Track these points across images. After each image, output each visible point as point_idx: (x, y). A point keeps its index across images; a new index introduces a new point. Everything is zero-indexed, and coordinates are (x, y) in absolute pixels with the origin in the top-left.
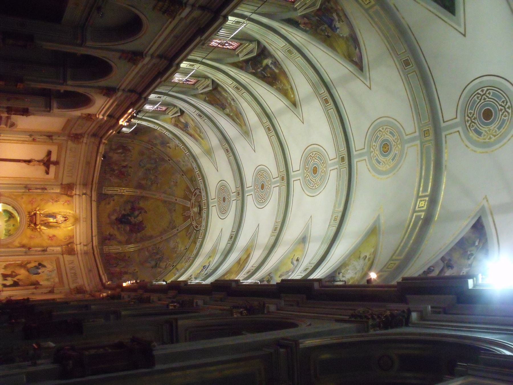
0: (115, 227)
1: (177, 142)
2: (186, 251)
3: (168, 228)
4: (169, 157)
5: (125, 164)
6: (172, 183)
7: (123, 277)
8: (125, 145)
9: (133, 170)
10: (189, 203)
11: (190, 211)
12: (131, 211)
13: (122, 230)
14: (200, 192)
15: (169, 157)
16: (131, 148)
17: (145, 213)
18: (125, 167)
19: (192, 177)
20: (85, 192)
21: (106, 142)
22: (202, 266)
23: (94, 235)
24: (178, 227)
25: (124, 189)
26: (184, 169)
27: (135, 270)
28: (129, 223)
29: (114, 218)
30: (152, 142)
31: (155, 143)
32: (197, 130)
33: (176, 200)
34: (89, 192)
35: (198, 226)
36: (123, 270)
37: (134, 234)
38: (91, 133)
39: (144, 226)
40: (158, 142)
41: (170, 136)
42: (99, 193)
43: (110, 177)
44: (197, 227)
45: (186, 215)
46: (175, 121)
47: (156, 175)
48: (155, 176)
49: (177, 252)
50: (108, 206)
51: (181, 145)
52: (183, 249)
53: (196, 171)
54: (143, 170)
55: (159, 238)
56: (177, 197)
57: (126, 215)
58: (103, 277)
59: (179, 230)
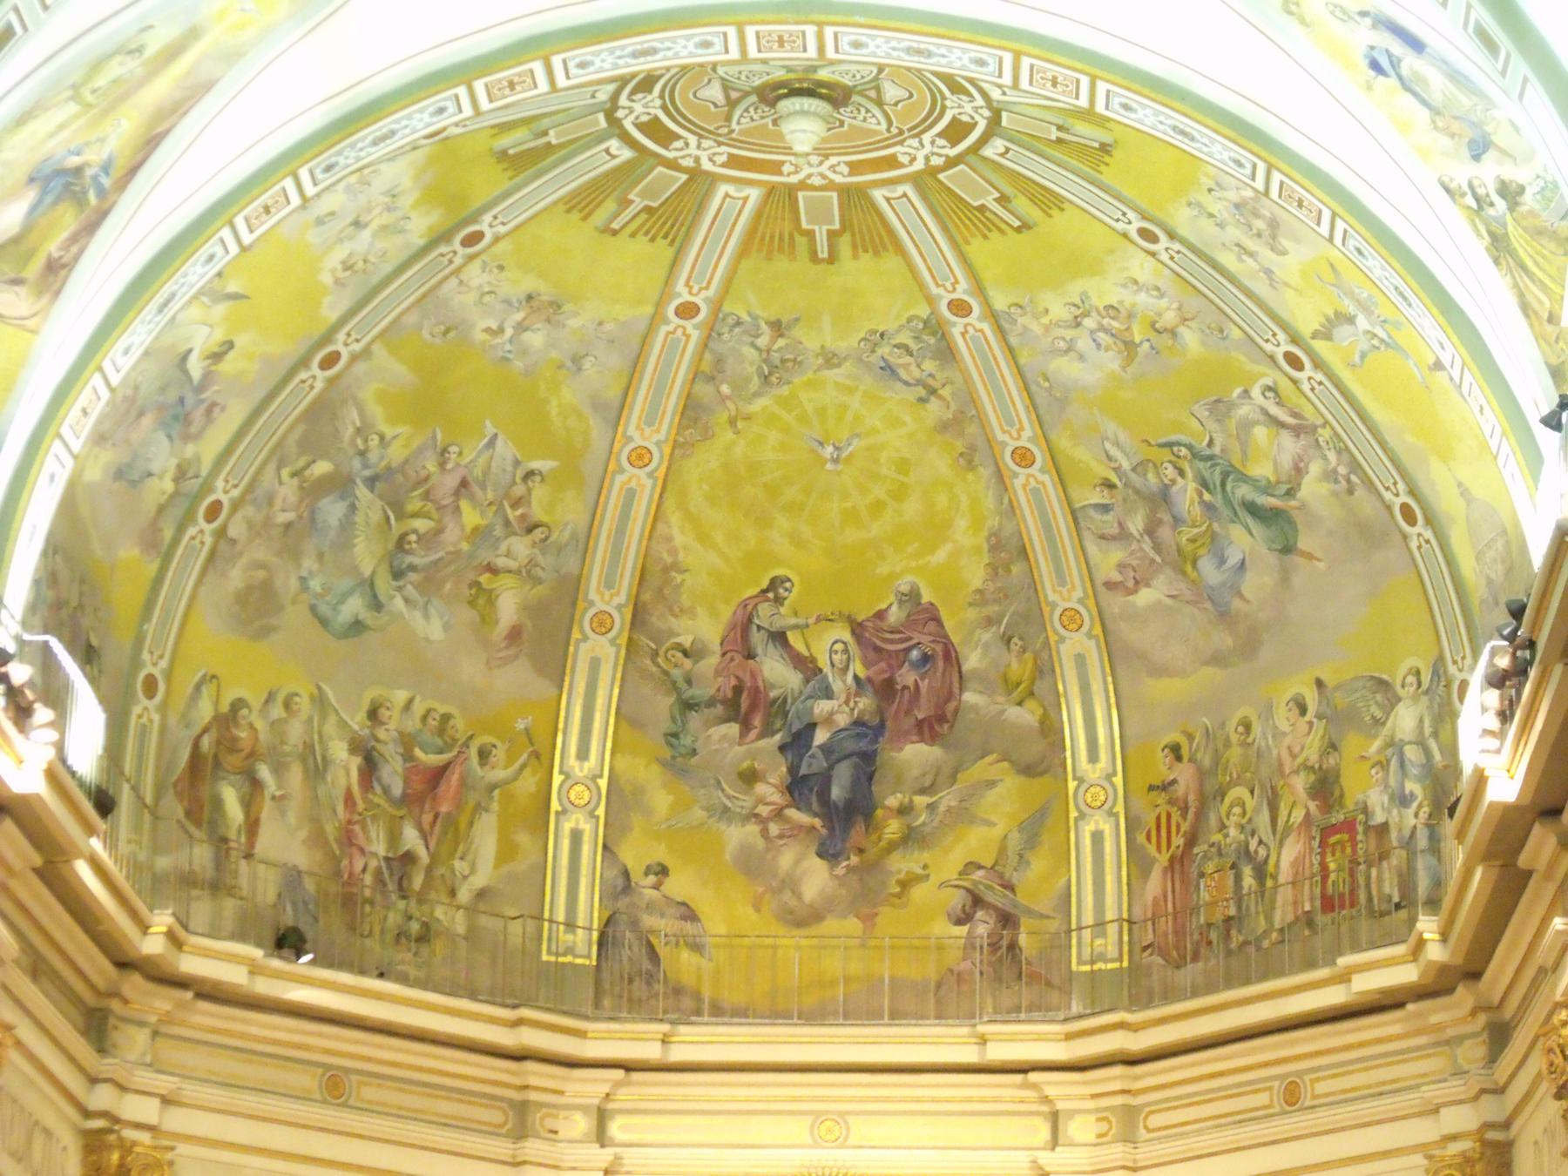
0: (902, 864)
1: (194, 273)
2: (1172, 236)
3: (933, 392)
4: (304, 363)
5: (345, 764)
6: (535, 339)
7: (1365, 810)
8: (185, 755)
9: (401, 696)
10: (730, 189)
11: (803, 185)
12: (757, 721)
13: (931, 807)
14: (646, 83)
15: (304, 363)
16: (205, 711)
17: (779, 601)
19: (503, 155)
20: (581, 1124)
21: (162, 921)
22: (1369, 87)
23: (970, 1055)
24: (931, 300)
25: (567, 775)
26: (419, 226)
27: (1303, 710)
29: (816, 878)
30: (161, 509)
31: (169, 486)
32: (115, 82)
33: (688, 311)
34: (589, 1087)
35: (955, 121)
36: (1298, 804)
37: (969, 697)
38: (81, 1047)
39: (895, 615)
40: (163, 458)
41: (139, 334)
42: (597, 1005)
43: (453, 893)
44: (957, 131)
45: (837, 226)
46: (17, 282)
47: (452, 481)
48: (457, 494)
49: (1170, 318)
50: (715, 923)
51: (221, 246)
52: (1140, 266)
53: (734, 54)
54: (399, 603)
55: (1021, 480)
56: (660, 305)
57: (793, 769)
58: (1367, 983)
59: (962, 291)
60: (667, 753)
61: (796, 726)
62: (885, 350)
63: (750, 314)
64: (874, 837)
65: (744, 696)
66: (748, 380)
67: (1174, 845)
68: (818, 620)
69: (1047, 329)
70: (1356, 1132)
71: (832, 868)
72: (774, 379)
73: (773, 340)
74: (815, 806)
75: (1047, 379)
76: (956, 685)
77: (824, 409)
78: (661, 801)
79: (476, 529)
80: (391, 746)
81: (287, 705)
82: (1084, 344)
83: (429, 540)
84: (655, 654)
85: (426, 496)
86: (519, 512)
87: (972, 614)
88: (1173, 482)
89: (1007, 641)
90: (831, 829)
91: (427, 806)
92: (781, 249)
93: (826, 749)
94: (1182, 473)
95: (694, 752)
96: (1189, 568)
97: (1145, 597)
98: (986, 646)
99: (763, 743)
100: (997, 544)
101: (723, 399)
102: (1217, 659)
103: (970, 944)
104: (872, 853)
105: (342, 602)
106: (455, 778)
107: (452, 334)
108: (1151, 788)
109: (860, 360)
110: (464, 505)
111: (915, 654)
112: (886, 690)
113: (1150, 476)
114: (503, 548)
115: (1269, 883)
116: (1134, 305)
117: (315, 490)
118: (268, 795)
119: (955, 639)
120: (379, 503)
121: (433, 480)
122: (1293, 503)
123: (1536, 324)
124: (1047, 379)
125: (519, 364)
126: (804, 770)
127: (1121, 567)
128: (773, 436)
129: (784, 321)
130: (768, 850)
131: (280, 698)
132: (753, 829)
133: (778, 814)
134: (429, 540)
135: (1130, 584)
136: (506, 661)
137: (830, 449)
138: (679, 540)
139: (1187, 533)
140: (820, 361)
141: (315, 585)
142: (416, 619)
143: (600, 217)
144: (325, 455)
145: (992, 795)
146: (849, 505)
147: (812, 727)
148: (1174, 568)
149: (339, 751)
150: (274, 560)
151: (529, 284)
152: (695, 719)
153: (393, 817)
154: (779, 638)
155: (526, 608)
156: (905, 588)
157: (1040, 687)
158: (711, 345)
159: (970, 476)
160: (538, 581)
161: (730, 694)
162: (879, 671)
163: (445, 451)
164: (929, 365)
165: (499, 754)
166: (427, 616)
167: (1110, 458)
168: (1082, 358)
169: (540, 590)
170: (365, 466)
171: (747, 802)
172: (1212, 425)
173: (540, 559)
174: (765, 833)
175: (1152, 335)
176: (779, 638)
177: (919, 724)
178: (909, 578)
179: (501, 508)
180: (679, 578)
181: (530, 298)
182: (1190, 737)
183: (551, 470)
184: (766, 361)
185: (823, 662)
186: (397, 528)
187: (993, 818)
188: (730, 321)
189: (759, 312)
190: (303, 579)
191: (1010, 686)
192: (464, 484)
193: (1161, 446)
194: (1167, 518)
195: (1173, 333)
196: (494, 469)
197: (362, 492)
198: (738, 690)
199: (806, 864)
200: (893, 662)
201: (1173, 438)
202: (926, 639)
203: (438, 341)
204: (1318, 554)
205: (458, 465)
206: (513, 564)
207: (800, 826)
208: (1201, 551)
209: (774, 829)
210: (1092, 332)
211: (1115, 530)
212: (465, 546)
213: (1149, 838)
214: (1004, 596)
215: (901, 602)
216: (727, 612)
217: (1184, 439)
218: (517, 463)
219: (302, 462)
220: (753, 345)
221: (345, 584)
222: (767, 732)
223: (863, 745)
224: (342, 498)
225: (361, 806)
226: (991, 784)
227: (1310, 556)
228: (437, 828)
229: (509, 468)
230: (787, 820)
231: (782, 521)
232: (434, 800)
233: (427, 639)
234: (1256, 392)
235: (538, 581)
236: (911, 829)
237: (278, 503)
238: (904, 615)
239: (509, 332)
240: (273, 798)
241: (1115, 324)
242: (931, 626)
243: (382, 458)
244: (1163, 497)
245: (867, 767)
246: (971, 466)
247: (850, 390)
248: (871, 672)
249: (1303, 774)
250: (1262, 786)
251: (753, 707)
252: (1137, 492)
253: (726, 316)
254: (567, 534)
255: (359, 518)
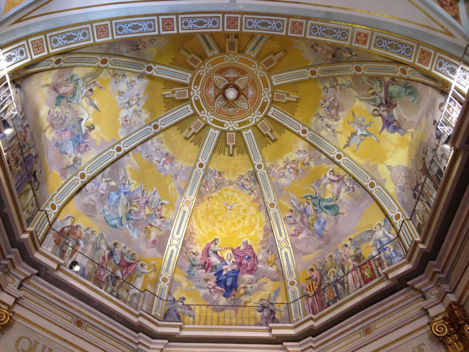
3: (252, 191)
9: (124, 245)
12: (209, 269)
13: (251, 287)
16: (69, 223)
17: (216, 244)
18: (111, 254)
28: (235, 275)
29: (223, 301)
37: (259, 266)
39: (242, 248)
47: (144, 201)
48: (145, 204)
57: (217, 279)
60: (187, 275)
61: (219, 270)
62: (242, 181)
63: (214, 169)
64: (237, 293)
65: (207, 264)
66: (212, 188)
67: (315, 288)
68: (225, 249)
69: (279, 170)
70: (395, 332)
71: (227, 299)
72: (218, 188)
73: (219, 177)
74: (223, 286)
75: (278, 185)
76: (256, 263)
77: (229, 196)
78: (185, 284)
79: (148, 214)
80: (118, 253)
81: (92, 232)
82: (287, 173)
83: (137, 213)
84: (187, 253)
85: (138, 202)
86: (159, 213)
87: (260, 246)
88: (307, 207)
89: (268, 252)
90: (227, 291)
91: (125, 269)
92: (222, 152)
93: (226, 275)
94: (309, 204)
95: (194, 275)
96: (311, 227)
97: (301, 236)
98: (263, 254)
99: (210, 273)
100: (265, 229)
101: (207, 192)
102: (320, 247)
103: (262, 317)
104: (237, 296)
105: (113, 220)
106: (133, 267)
107: (149, 158)
108: (306, 280)
109: (237, 183)
110: (146, 207)
111: (246, 257)
112: (240, 264)
113: (301, 206)
114: (154, 221)
115: (346, 285)
116: (299, 158)
117: (111, 189)
118: (80, 247)
119: (256, 253)
120: (126, 200)
121: (140, 199)
122: (338, 201)
123: (446, 8)
124: (278, 185)
125: (163, 173)
126: (220, 279)
127: (295, 230)
128: (217, 203)
129: (222, 171)
130: (211, 295)
131: (91, 230)
132: (207, 291)
133: (214, 288)
134: (137, 213)
135: (297, 234)
136: (151, 247)
137: (229, 207)
138: (194, 227)
139: (310, 218)
140: (228, 184)
141: (107, 213)
142: (131, 232)
143: (184, 134)
144: (115, 181)
145: (266, 285)
146: (232, 221)
147: (223, 271)
148: (308, 228)
149: (104, 247)
150: (97, 202)
151: (168, 150)
152: (194, 269)
153: (115, 267)
154: (216, 252)
155: (158, 236)
156: (244, 241)
157: (276, 262)
158: (205, 177)
159: (260, 213)
160: (161, 231)
161: (203, 264)
162: (238, 260)
163: (143, 192)
164: (252, 184)
165: (146, 267)
166: (133, 232)
167: (292, 204)
168: (286, 177)
169: (161, 233)
170: (124, 188)
171: (206, 285)
172: (316, 188)
173: (162, 225)
174: (210, 291)
175: (303, 166)
176: (216, 252)
177: (248, 271)
178: (245, 239)
179: (155, 211)
180: (194, 236)
181: (167, 154)
182: (315, 266)
183: (168, 204)
184: (217, 183)
185: (225, 258)
186: (130, 208)
187: (267, 290)
188: (210, 171)
189: (216, 169)
190: (103, 210)
191: (269, 262)
192: (147, 202)
193: (304, 198)
194: (305, 216)
195: (308, 164)
196: (154, 200)
197: (122, 195)
198: (205, 263)
199: (220, 298)
200: (242, 258)
201: (307, 195)
202: (249, 253)
203: (145, 158)
204: (344, 212)
205: (146, 197)
206: (156, 225)
207: (219, 290)
208: (315, 222)
209: (212, 290)
210: (289, 169)
211: (293, 222)
212: (145, 218)
213: (307, 290)
214: (267, 241)
215: (243, 244)
216: (204, 246)
217: (309, 194)
218: (160, 200)
219: (108, 179)
220: (214, 178)
221: (114, 216)
222: (212, 271)
223: (234, 274)
224: (117, 194)
225: (106, 261)
226: (266, 283)
227: (343, 213)
228: (127, 275)
229: (158, 201)
230: (216, 289)
231: (217, 225)
232: (127, 269)
233: (132, 237)
234: (328, 174)
235: (161, 231)
236: (246, 291)
237: (100, 188)
238: (244, 247)
239: (162, 163)
240: (82, 248)
241: (294, 165)
242: (250, 250)
243: (128, 188)
244: (305, 210)
245: (235, 278)
246: (260, 210)
247: (234, 192)
248: (236, 260)
249: (350, 258)
250: (338, 265)
251: (209, 266)
252: (298, 211)
253: (210, 169)
254: (169, 221)
255: (121, 201)
